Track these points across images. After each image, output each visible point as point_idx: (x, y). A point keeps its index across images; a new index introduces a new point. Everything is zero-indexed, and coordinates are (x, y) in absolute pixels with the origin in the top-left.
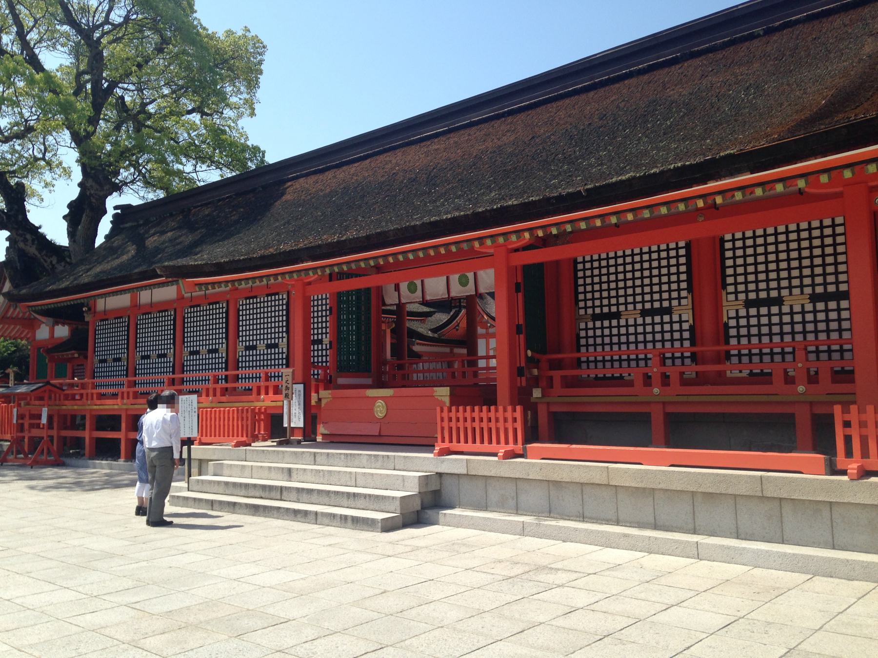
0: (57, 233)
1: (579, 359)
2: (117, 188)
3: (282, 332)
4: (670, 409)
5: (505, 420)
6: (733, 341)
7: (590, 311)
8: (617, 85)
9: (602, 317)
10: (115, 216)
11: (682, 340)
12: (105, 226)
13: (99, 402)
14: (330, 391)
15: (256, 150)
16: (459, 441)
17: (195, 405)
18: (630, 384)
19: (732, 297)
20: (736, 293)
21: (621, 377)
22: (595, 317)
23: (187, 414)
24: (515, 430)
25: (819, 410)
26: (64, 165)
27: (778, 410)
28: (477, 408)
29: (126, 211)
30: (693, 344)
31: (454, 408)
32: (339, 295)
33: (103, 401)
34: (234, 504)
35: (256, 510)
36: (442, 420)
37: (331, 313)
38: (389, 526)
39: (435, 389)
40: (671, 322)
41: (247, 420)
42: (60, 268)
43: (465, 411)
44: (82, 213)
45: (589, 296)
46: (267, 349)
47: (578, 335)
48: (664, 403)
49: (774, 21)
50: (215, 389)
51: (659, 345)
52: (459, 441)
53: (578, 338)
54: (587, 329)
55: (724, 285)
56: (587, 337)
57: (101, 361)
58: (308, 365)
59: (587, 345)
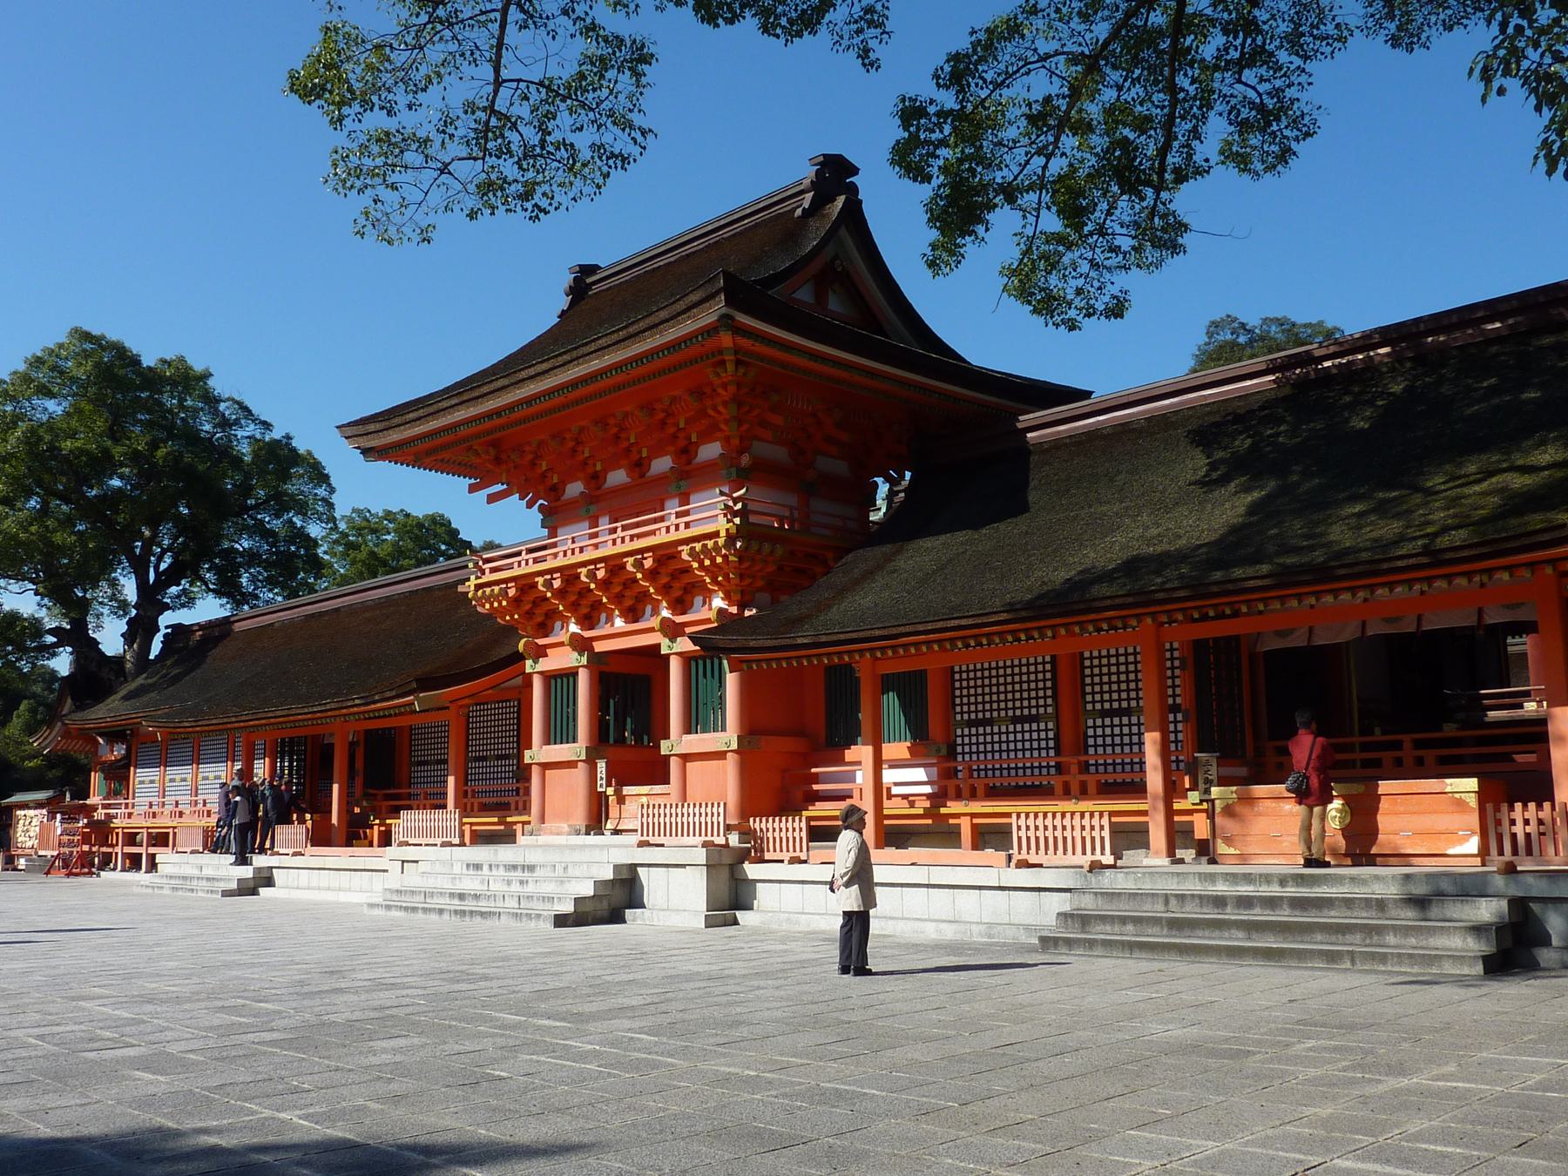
4: (976, 821)
9: (1111, 713)
10: (165, 636)
12: (156, 647)
28: (1518, 806)
29: (178, 629)
30: (1058, 753)
35: (1269, 954)
36: (1019, 828)
39: (1448, 781)
45: (1097, 688)
51: (967, 757)
53: (1086, 737)
54: (1095, 727)
56: (1095, 736)
59: (1096, 746)
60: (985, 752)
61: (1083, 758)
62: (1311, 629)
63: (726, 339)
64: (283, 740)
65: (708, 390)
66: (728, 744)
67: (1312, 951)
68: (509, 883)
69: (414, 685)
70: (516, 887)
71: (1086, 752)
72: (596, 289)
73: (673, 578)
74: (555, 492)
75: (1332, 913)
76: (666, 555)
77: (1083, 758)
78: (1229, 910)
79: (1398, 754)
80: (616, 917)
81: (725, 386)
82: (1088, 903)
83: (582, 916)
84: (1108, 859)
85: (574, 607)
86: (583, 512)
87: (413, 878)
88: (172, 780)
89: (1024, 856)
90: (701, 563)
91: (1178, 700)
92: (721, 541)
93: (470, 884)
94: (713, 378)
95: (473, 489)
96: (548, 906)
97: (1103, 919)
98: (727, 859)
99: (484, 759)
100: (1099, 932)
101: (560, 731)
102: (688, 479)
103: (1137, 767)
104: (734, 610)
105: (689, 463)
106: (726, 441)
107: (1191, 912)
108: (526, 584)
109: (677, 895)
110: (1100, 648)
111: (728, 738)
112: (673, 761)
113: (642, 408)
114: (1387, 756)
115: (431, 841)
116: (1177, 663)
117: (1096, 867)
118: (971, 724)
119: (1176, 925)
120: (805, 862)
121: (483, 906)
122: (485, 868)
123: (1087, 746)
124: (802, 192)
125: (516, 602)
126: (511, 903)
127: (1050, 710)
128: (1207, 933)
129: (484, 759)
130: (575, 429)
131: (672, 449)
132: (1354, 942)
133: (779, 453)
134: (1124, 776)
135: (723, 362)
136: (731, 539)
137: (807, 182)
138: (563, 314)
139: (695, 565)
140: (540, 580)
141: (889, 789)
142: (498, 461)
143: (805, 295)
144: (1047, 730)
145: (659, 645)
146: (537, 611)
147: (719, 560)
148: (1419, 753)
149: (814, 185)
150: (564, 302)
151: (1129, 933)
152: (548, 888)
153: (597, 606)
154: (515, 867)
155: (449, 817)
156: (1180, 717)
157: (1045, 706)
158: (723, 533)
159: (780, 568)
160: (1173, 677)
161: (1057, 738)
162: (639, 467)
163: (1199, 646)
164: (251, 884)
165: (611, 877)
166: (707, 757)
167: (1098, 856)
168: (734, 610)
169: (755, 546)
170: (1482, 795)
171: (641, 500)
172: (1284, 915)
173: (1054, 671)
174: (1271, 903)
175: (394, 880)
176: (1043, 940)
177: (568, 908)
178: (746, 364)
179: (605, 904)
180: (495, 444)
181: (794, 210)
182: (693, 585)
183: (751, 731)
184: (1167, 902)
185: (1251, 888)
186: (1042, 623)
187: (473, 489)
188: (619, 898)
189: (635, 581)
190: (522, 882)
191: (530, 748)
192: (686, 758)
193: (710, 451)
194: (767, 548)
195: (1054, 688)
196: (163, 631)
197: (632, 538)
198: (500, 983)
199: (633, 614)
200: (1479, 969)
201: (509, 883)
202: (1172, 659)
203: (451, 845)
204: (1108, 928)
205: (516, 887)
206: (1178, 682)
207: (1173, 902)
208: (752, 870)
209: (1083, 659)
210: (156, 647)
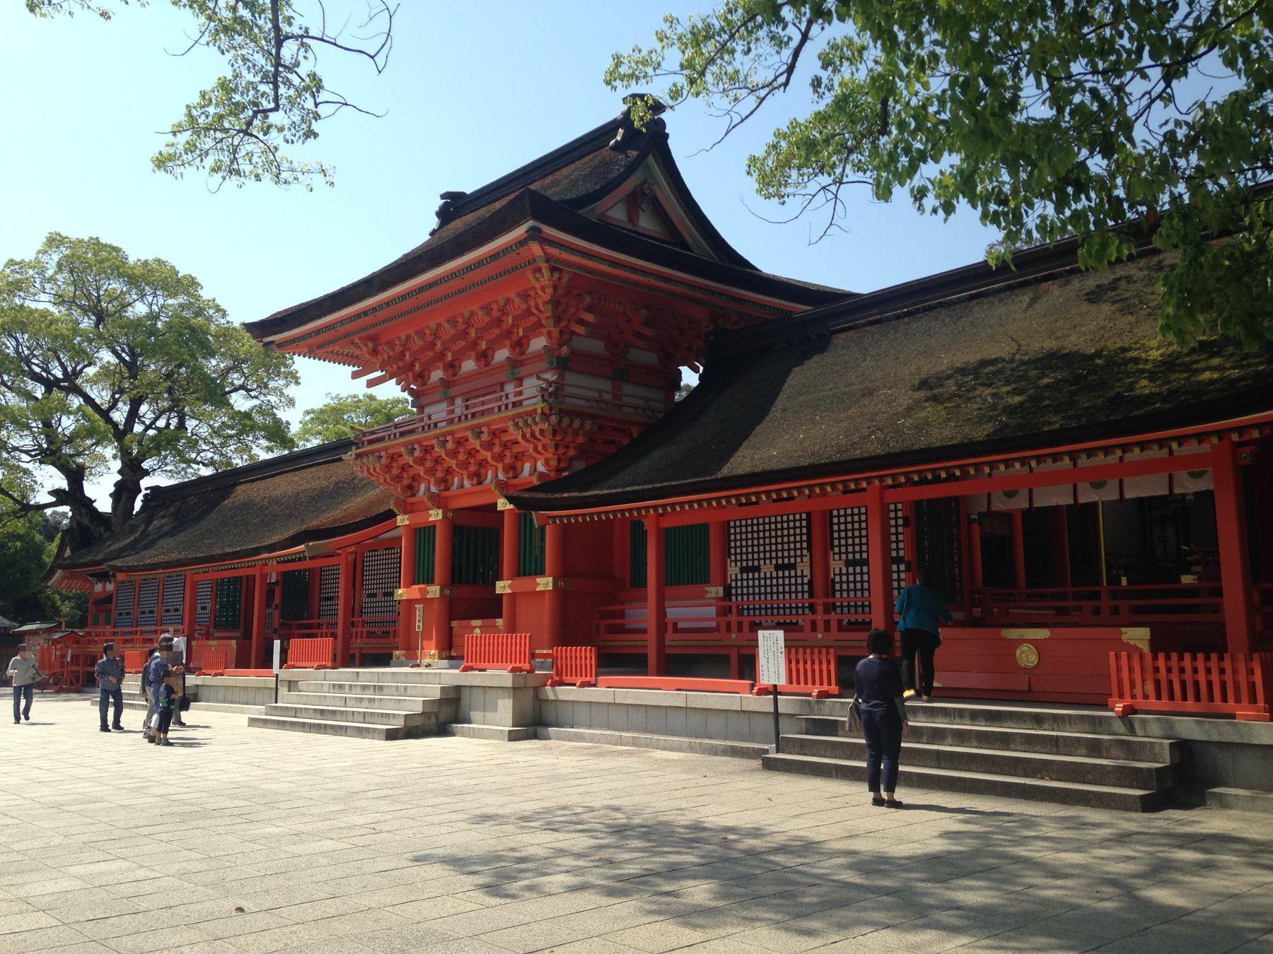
0: (104, 505)
1: (834, 604)
2: (146, 473)
6: (838, 594)
8: (1000, 309)
10: (145, 496)
11: (803, 592)
12: (138, 505)
17: (782, 643)
18: (801, 629)
19: (837, 557)
20: (840, 553)
21: (797, 623)
23: (771, 655)
24: (829, 672)
25: (743, 652)
27: (718, 652)
29: (155, 490)
30: (811, 596)
32: (918, 504)
33: (614, 636)
34: (284, 722)
37: (906, 525)
38: (392, 735)
40: (796, 577)
41: (829, 663)
42: (106, 536)
44: (124, 492)
46: (742, 573)
48: (739, 647)
50: (827, 623)
55: (832, 547)
57: (370, 596)
58: (193, 621)
60: (778, 593)
61: (830, 600)
62: (989, 495)
63: (535, 248)
65: (532, 293)
74: (421, 377)
77: (830, 600)
88: (176, 610)
91: (902, 553)
94: (534, 282)
95: (355, 375)
101: (422, 575)
103: (867, 609)
112: (504, 599)
113: (482, 308)
116: (900, 522)
123: (834, 591)
134: (856, 616)
135: (539, 269)
138: (433, 233)
141: (675, 624)
142: (375, 352)
143: (618, 214)
155: (325, 644)
156: (902, 567)
158: (539, 411)
159: (592, 440)
160: (897, 534)
169: (566, 421)
177: (398, 724)
180: (374, 338)
182: (523, 453)
186: (779, 486)
187: (355, 375)
196: (144, 492)
198: (289, 804)
202: (896, 518)
203: (325, 667)
209: (832, 517)
210: (138, 505)
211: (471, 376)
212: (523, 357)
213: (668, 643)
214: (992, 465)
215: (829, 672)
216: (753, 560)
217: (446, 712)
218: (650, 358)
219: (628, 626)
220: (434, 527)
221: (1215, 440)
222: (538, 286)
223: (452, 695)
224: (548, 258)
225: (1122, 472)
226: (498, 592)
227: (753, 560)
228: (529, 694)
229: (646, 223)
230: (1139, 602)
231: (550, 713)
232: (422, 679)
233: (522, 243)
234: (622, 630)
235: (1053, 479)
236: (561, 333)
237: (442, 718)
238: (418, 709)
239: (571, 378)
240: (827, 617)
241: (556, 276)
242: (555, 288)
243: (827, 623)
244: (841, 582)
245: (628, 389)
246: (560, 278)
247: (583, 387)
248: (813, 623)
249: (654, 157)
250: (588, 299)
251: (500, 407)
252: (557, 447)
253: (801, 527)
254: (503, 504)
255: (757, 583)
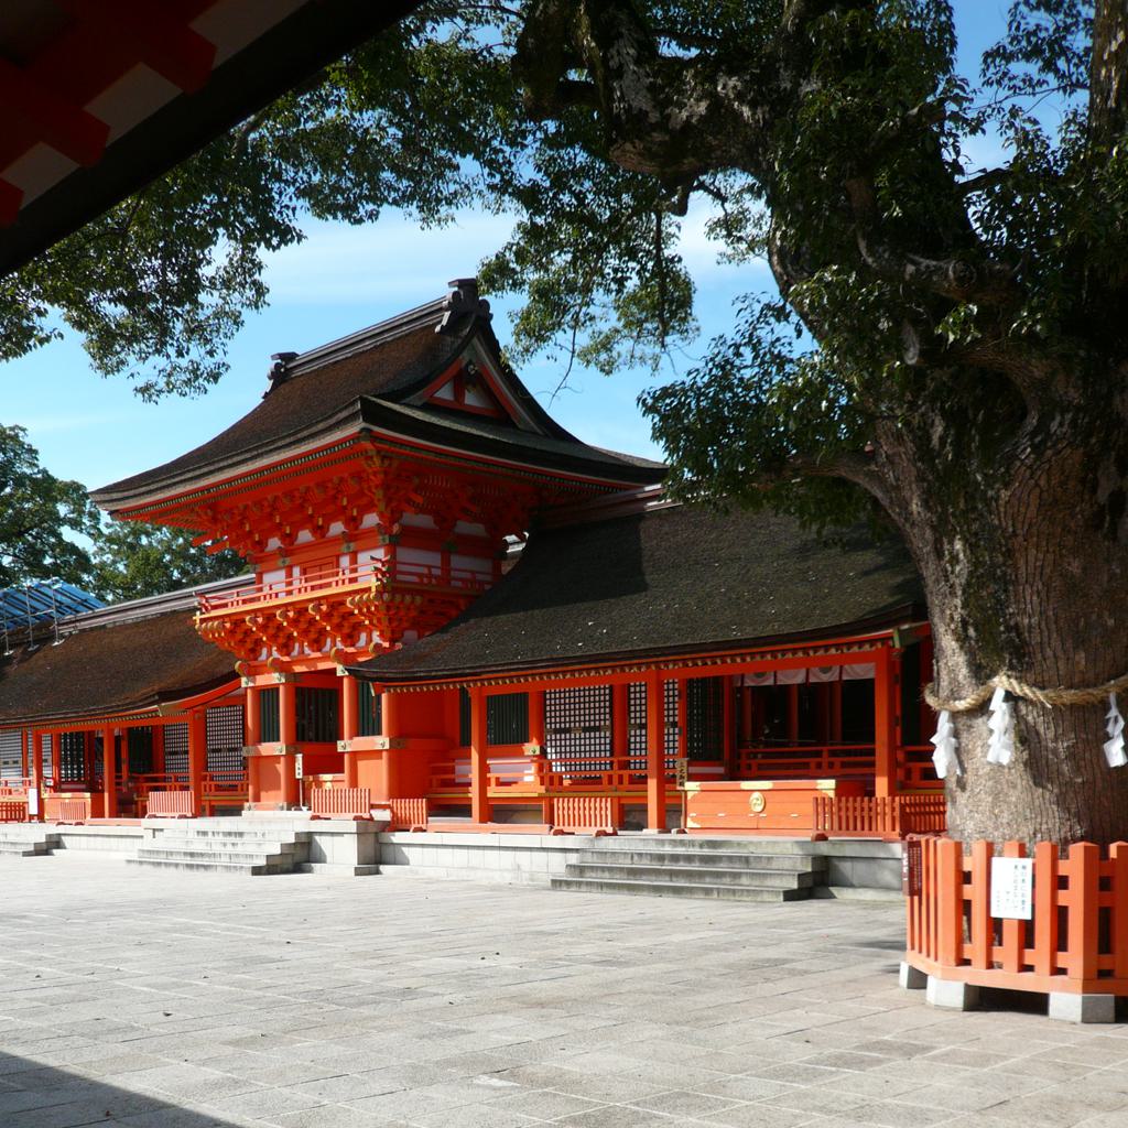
1: (629, 763)
3: (605, 714)
5: (847, 809)
7: (638, 721)
13: (236, 783)
14: (698, 783)
15: (32, 452)
16: (569, 825)
22: (598, 729)
26: (539, 350)
30: (612, 755)
31: (844, 799)
35: (677, 891)
37: (679, 696)
39: (819, 781)
43: (862, 801)
47: (629, 740)
49: (655, 506)
50: (621, 777)
52: (569, 825)
53: (630, 743)
64: (71, 734)
65: (364, 475)
66: (383, 745)
67: (643, 885)
68: (225, 845)
69: (157, 697)
70: (229, 848)
71: (629, 754)
72: (298, 373)
73: (340, 617)
75: (722, 865)
76: (336, 603)
78: (666, 862)
79: (819, 760)
80: (298, 868)
81: (375, 474)
82: (590, 860)
83: (272, 868)
84: (610, 830)
85: (273, 638)
86: (280, 563)
87: (160, 843)
89: (561, 827)
90: (360, 610)
92: (372, 595)
93: (199, 846)
96: (249, 860)
97: (592, 868)
98: (372, 828)
99: (219, 750)
100: (590, 877)
102: (356, 538)
103: (643, 765)
104: (386, 645)
105: (263, 551)
106: (381, 515)
107: (646, 864)
108: (237, 621)
109: (342, 851)
110: (638, 679)
111: (381, 742)
112: (346, 757)
114: (813, 761)
115: (70, 822)
116: (676, 693)
117: (601, 834)
118: (556, 731)
119: (633, 872)
120: (425, 831)
121: (205, 861)
122: (210, 834)
124: (441, 309)
125: (232, 632)
126: (225, 860)
127: (608, 723)
128: (618, 876)
129: (219, 750)
130: (241, 506)
131: (343, 518)
132: (726, 882)
133: (424, 521)
136: (380, 592)
137: (445, 303)
138: (266, 396)
139: (356, 612)
140: (247, 618)
142: (215, 520)
144: (605, 738)
145: (335, 669)
146: (346, 624)
147: (373, 609)
148: (832, 759)
149: (451, 306)
150: (267, 385)
151: (606, 878)
152: (251, 849)
153: (322, 633)
154: (230, 834)
157: (605, 720)
158: (374, 589)
159: (422, 612)
161: (612, 743)
162: (320, 531)
163: (690, 684)
164: (45, 847)
165: (293, 841)
166: (370, 751)
167: (604, 828)
168: (386, 645)
169: (398, 598)
170: (838, 790)
171: (320, 561)
172: (695, 867)
173: (611, 694)
174: (689, 858)
175: (149, 843)
176: (554, 881)
177: (262, 862)
178: (391, 459)
179: (290, 860)
181: (435, 325)
183: (398, 736)
184: (632, 857)
185: (684, 849)
188: (300, 857)
189: (352, 614)
190: (233, 844)
191: (343, 739)
192: (355, 755)
193: (371, 520)
194: (408, 598)
195: (611, 707)
197: (313, 588)
199: (317, 644)
200: (782, 898)
201: (225, 845)
203: (185, 817)
204: (594, 875)
205: (229, 849)
206: (676, 712)
207: (636, 858)
208: (398, 837)
209: (545, 693)
211: (308, 546)
212: (356, 532)
213: (489, 795)
214: (733, 657)
215: (606, 816)
216: (595, 720)
217: (300, 854)
218: (478, 529)
219: (457, 781)
220: (278, 689)
221: (879, 645)
222: (370, 471)
223: (304, 840)
224: (379, 451)
225: (842, 662)
226: (340, 750)
227: (595, 720)
228: (371, 838)
229: (471, 399)
230: (845, 759)
231: (388, 853)
232: (270, 823)
233: (355, 438)
234: (452, 784)
235: (796, 665)
236: (392, 512)
237: (297, 858)
238: (278, 851)
239: (404, 554)
240: (621, 772)
241: (387, 463)
242: (386, 473)
243: (621, 777)
244: (635, 742)
245: (457, 561)
246: (390, 465)
247: (419, 561)
248: (610, 777)
249: (479, 340)
250: (416, 481)
251: (337, 582)
252: (390, 620)
253: (605, 701)
254: (340, 671)
255: (573, 749)
